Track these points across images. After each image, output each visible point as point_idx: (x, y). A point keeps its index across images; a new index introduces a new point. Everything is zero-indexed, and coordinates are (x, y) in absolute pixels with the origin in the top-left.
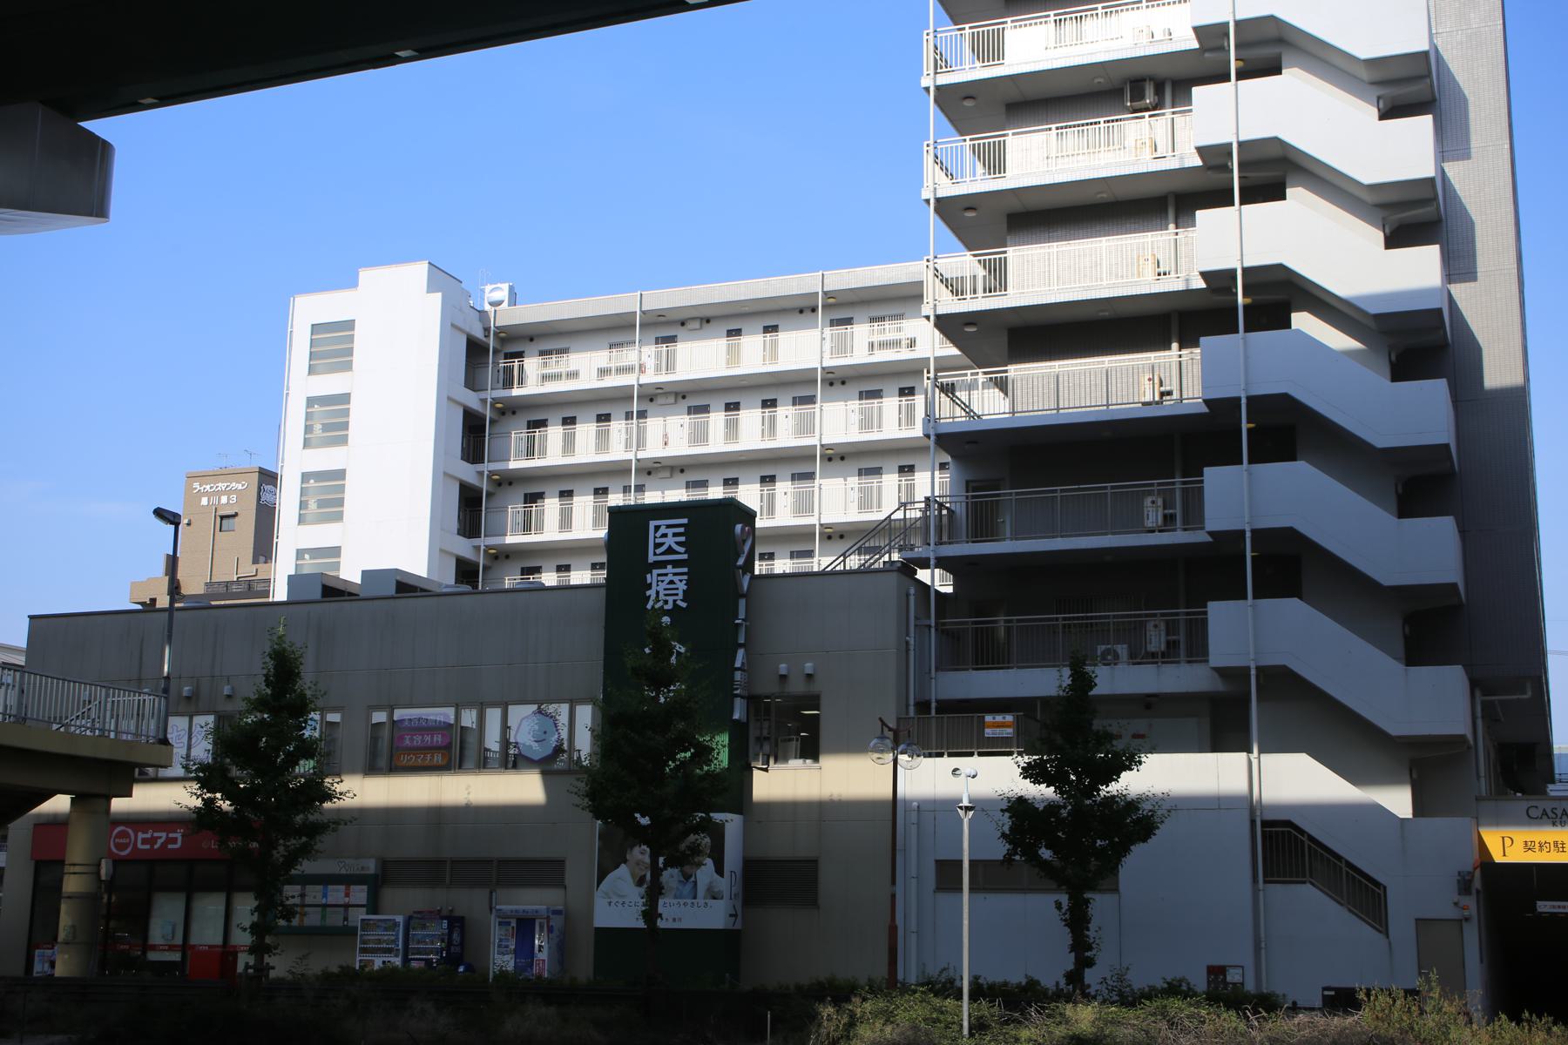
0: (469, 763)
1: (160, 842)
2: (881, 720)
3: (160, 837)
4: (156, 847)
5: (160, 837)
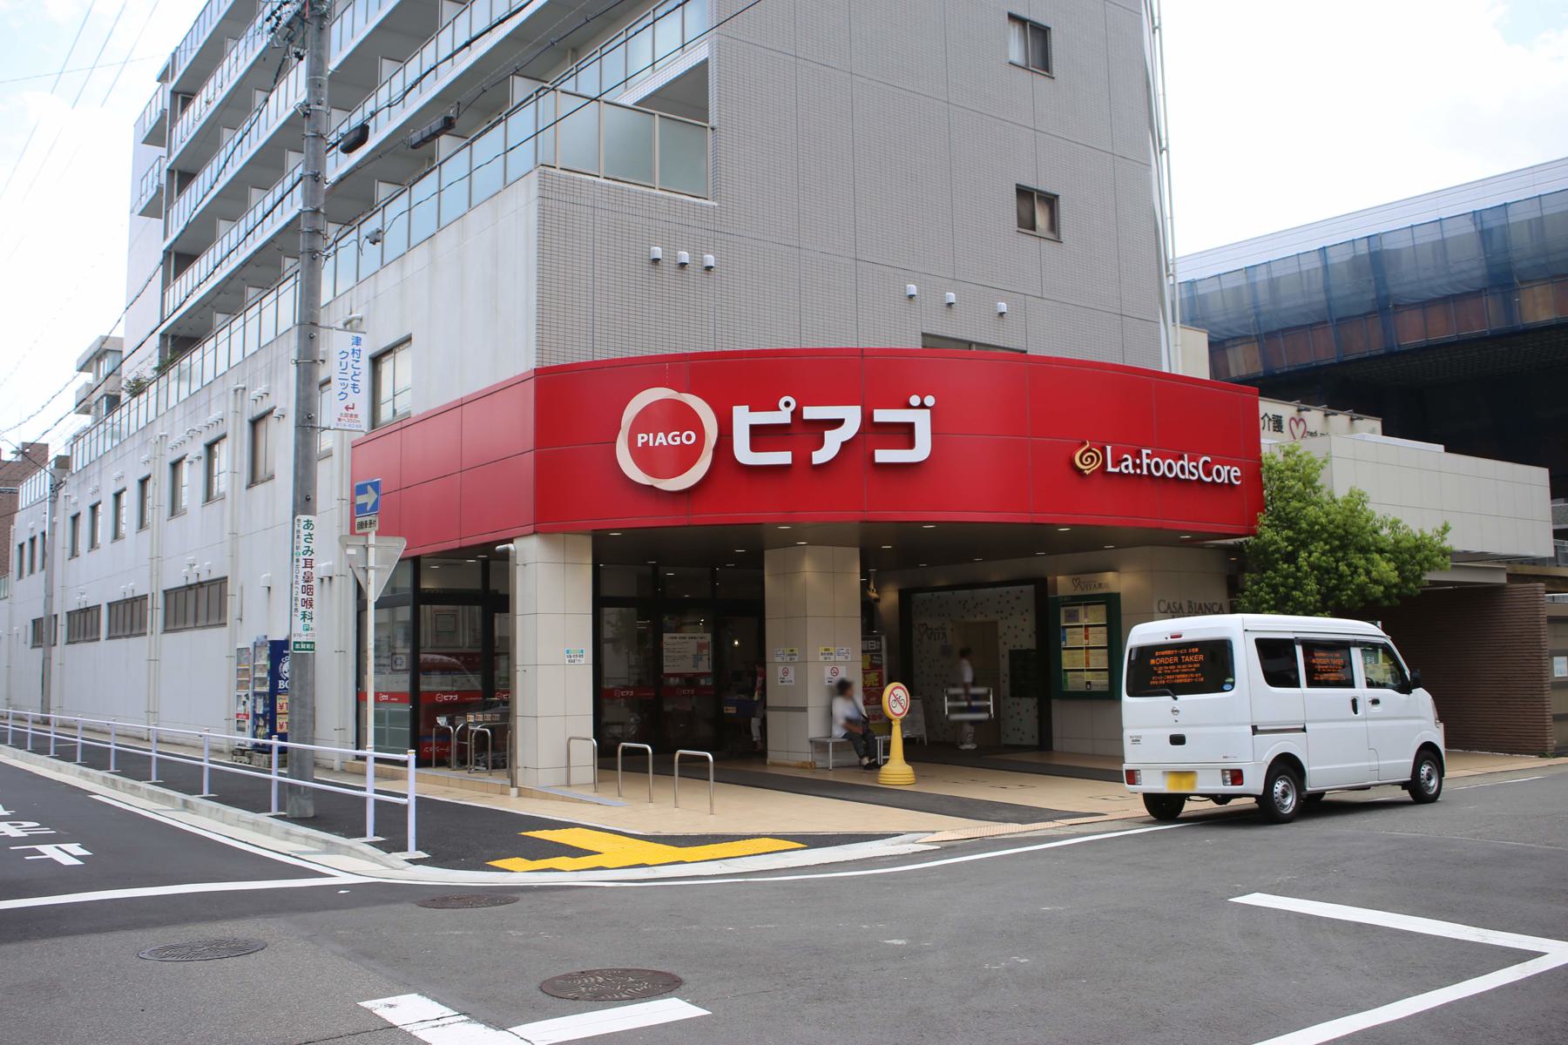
0: (201, 622)
1: (832, 443)
2: (1013, 17)
3: (837, 423)
4: (820, 457)
5: (837, 423)
